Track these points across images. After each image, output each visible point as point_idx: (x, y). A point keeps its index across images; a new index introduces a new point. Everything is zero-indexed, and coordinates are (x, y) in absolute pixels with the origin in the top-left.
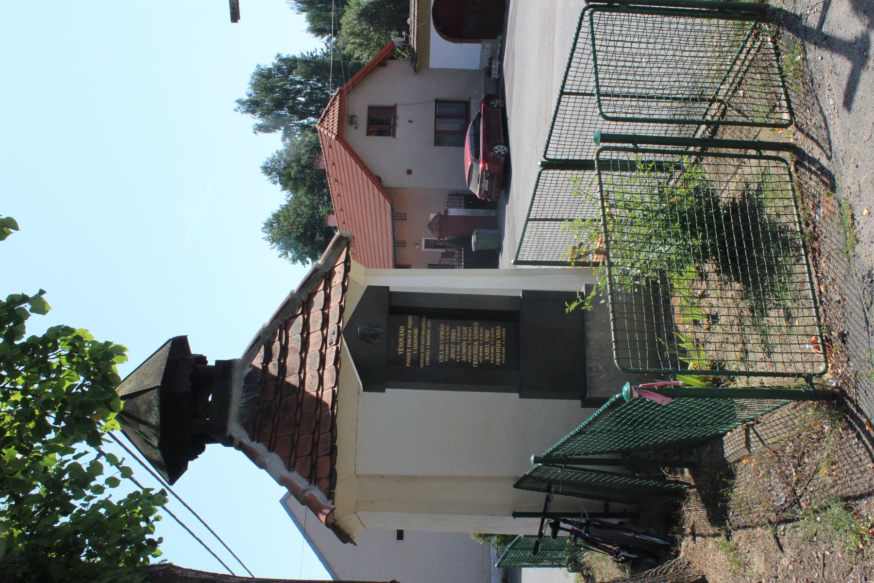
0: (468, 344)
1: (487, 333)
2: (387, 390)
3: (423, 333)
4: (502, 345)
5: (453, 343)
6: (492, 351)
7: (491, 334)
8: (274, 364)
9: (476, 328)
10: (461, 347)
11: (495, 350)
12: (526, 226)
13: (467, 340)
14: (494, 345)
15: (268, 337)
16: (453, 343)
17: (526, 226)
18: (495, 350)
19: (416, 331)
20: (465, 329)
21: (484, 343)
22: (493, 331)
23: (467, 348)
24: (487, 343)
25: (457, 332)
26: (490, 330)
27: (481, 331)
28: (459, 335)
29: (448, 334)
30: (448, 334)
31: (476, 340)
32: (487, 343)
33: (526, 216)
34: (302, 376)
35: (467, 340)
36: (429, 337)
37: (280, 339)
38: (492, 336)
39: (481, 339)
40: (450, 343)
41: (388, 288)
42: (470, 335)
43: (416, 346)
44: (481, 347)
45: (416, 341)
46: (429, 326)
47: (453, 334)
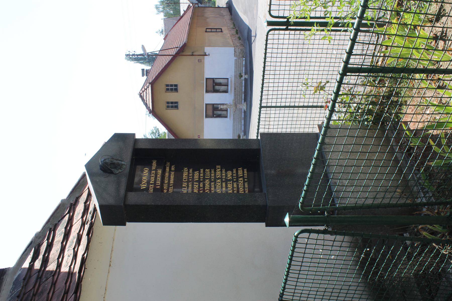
0: (211, 181)
1: (229, 173)
2: (127, 223)
3: (167, 174)
4: (244, 182)
5: (196, 181)
6: (235, 186)
7: (233, 173)
8: (39, 260)
9: (219, 184)
10: (204, 185)
11: (238, 185)
12: (260, 112)
13: (210, 179)
14: (237, 181)
15: (39, 241)
16: (196, 181)
17: (260, 112)
18: (238, 185)
19: (160, 172)
20: (207, 170)
21: (227, 181)
22: (235, 172)
23: (210, 184)
24: (230, 180)
25: (200, 173)
26: (232, 171)
27: (224, 172)
28: (202, 175)
29: (191, 175)
30: (191, 175)
31: (218, 179)
32: (230, 180)
33: (259, 106)
34: (60, 260)
35: (210, 179)
36: (172, 177)
37: (48, 239)
38: (235, 175)
39: (224, 177)
40: (193, 181)
41: (134, 135)
42: (213, 175)
43: (159, 182)
44: (224, 184)
45: (159, 179)
46: (173, 169)
47: (195, 175)
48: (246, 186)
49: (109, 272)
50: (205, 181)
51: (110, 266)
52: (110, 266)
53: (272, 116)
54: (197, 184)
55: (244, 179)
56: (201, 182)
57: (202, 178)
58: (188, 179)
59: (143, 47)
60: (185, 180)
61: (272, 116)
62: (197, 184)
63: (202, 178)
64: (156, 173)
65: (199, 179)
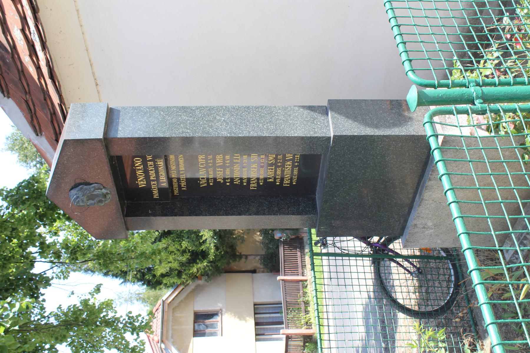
4: (293, 166)
5: (220, 167)
14: (283, 166)
16: (220, 167)
48: (296, 172)
49: (99, 93)
50: (233, 166)
51: (97, 85)
52: (97, 85)
53: (354, 269)
54: (221, 171)
55: (293, 163)
56: (228, 167)
57: (228, 162)
58: (207, 163)
59: (111, 116)
60: (202, 164)
61: (354, 269)
62: (221, 171)
63: (228, 162)
64: (155, 165)
65: (224, 162)
